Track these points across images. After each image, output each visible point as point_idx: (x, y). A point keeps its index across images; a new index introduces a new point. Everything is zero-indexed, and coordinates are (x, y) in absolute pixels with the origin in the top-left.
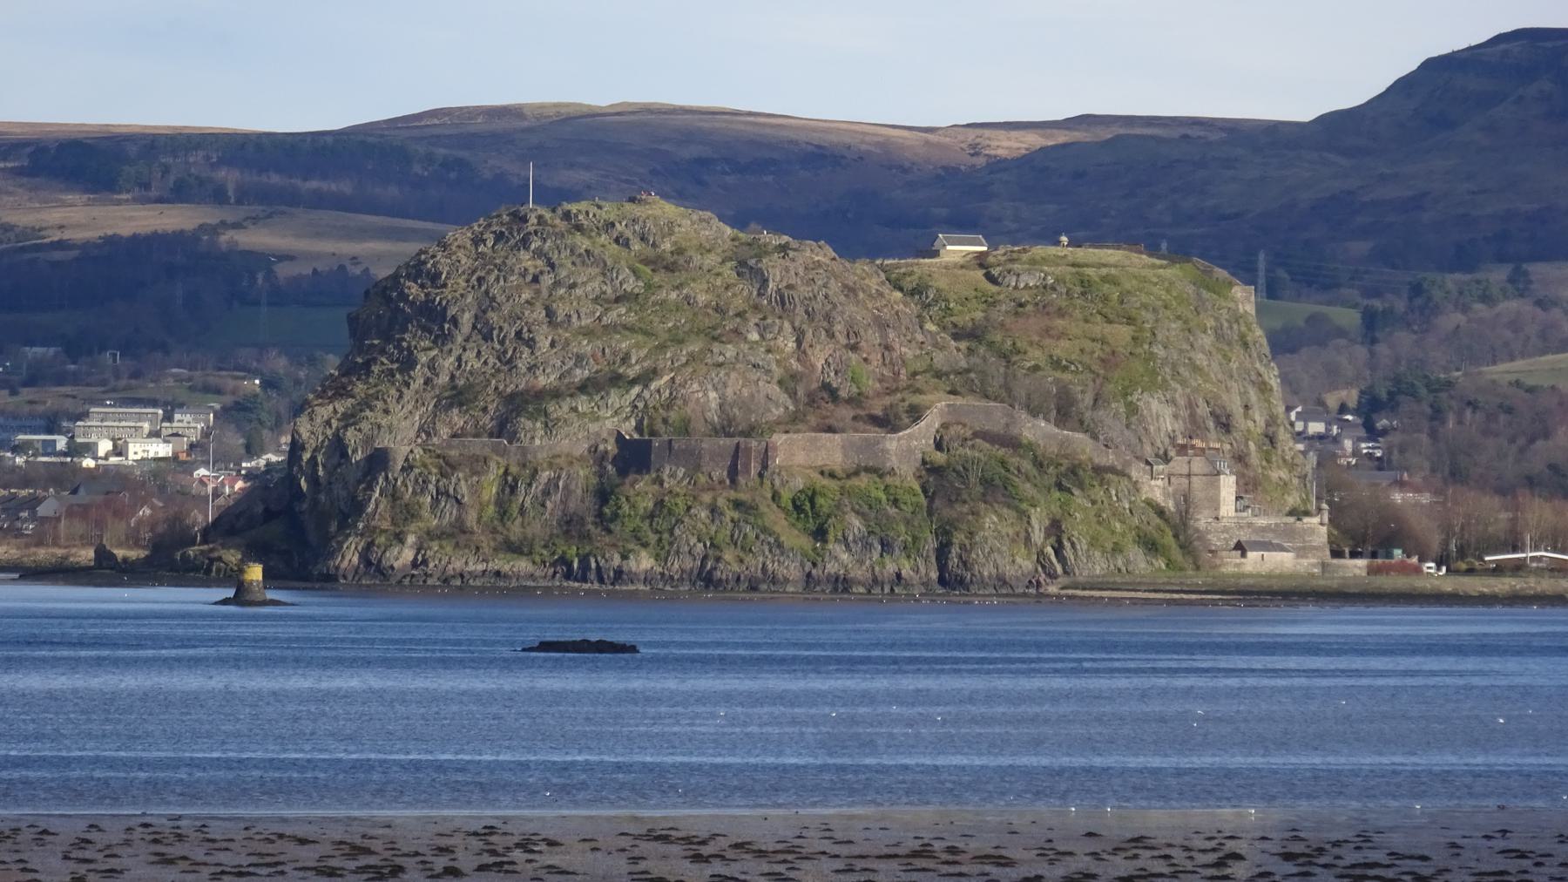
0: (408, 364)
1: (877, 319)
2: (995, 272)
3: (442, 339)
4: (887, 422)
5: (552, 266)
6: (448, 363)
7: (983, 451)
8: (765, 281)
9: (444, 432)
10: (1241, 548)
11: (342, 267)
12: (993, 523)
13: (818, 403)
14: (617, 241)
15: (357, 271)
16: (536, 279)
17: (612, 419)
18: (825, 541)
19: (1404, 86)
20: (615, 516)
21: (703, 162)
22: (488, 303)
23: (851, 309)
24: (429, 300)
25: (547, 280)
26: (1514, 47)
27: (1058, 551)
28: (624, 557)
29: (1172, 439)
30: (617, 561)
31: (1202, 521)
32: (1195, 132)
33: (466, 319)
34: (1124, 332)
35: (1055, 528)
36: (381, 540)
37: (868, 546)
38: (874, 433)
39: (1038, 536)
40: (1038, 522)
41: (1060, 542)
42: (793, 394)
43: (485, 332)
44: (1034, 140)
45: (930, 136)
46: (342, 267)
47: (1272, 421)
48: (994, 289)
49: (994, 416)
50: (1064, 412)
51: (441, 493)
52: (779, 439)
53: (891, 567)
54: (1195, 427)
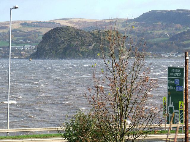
17: (65, 45)
33: (52, 37)
35: (104, 54)
43: (54, 38)
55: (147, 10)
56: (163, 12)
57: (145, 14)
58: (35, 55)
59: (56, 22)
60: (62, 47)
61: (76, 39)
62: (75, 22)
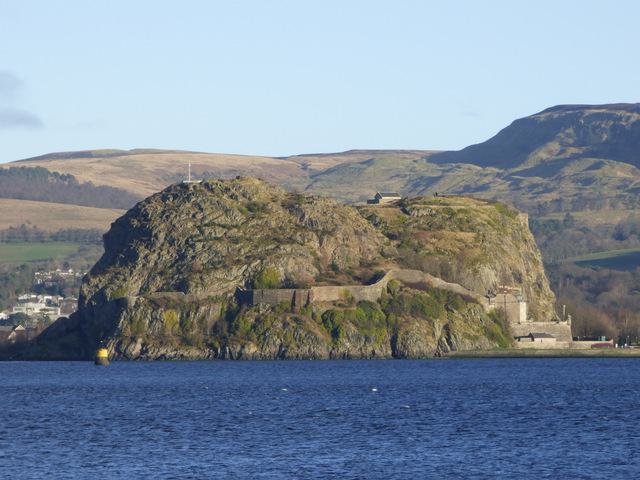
2: (408, 209)
3: (150, 245)
5: (202, 210)
6: (154, 257)
12: (418, 326)
13: (330, 274)
14: (231, 197)
17: (232, 280)
19: (505, 133)
25: (199, 216)
27: (448, 340)
29: (495, 286)
33: (162, 236)
34: (469, 236)
35: (446, 328)
39: (438, 333)
40: (439, 325)
45: (285, 162)
47: (539, 276)
49: (416, 276)
50: (445, 274)
51: (154, 319)
52: (315, 289)
54: (505, 281)
55: (532, 105)
56: (619, 113)
57: (517, 123)
58: (68, 331)
59: (52, 166)
60: (215, 290)
61: (288, 248)
62: (150, 167)
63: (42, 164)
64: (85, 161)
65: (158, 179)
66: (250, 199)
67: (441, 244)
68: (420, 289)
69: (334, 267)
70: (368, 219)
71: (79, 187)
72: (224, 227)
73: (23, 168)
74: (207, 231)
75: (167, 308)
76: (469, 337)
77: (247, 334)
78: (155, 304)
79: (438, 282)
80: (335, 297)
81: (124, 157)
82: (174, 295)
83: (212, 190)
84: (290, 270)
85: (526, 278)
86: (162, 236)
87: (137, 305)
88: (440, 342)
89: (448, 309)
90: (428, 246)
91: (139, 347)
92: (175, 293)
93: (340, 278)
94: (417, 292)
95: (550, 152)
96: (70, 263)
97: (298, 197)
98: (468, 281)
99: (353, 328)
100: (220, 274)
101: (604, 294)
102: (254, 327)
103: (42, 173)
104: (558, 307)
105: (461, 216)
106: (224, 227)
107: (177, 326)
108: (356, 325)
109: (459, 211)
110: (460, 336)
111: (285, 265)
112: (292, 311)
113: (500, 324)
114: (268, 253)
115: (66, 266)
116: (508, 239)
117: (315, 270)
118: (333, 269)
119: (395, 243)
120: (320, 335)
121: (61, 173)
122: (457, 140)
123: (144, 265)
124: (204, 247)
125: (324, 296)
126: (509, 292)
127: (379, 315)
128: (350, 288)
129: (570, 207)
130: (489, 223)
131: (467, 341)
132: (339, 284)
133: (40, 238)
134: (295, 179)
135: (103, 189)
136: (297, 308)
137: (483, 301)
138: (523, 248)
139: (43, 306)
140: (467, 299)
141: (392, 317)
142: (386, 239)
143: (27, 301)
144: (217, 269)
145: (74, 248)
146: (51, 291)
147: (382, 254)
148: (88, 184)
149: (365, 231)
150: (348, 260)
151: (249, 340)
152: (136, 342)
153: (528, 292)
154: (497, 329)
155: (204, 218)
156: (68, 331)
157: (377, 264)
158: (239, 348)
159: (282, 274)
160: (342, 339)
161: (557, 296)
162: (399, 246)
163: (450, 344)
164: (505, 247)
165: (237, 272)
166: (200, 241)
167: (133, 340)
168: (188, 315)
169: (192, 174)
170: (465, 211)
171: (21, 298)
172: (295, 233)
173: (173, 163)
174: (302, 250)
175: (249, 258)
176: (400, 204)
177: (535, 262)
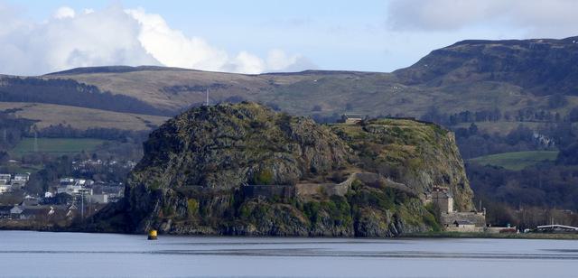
0: (166, 159)
1: (329, 144)
2: (367, 127)
3: (177, 151)
4: (337, 180)
5: (217, 126)
6: (180, 160)
7: (369, 190)
8: (291, 131)
9: (180, 183)
10: (457, 224)
11: (61, 125)
13: (310, 173)
14: (238, 117)
15: (66, 125)
16: (211, 130)
17: (237, 179)
18: (315, 222)
19: (425, 60)
20: (241, 213)
21: (177, 87)
22: (194, 139)
23: (321, 140)
24: (173, 137)
25: (215, 130)
26: (463, 46)
28: (245, 226)
29: (430, 185)
30: (242, 229)
31: (443, 214)
32: (174, 74)
33: (187, 144)
34: (411, 148)
35: (395, 216)
36: (160, 221)
37: (330, 223)
38: (329, 184)
39: (389, 220)
40: (389, 213)
41: (396, 221)
42: (302, 171)
43: (193, 148)
44: (292, 80)
46: (61, 125)
47: (462, 179)
48: (366, 133)
49: (373, 177)
50: (394, 175)
52: (299, 186)
53: (338, 230)
54: (438, 182)
59: (79, 78)
61: (280, 155)
63: (73, 77)
64: (104, 75)
65: (160, 90)
66: (251, 118)
67: (391, 154)
68: (376, 187)
69: (313, 170)
70: (338, 134)
71: (101, 95)
72: (233, 138)
73: (59, 80)
74: (220, 141)
75: (190, 198)
76: (411, 223)
77: (249, 218)
78: (181, 195)
79: (389, 182)
80: (314, 192)
81: (133, 73)
82: (194, 188)
83: (224, 112)
84: (281, 172)
85: (452, 180)
86: (187, 144)
87: (168, 196)
88: (390, 225)
89: (396, 203)
90: (381, 155)
91: (168, 226)
92: (195, 186)
93: (318, 178)
94: (374, 189)
95: (459, 76)
96: (98, 154)
97: (288, 118)
98: (411, 182)
99: (326, 214)
100: (229, 173)
101: (502, 187)
102: (254, 213)
103: (74, 83)
104: (475, 201)
105: (406, 133)
106: (233, 138)
107: (197, 210)
108: (329, 213)
109: (405, 130)
110: (405, 222)
111: (277, 169)
112: (282, 202)
113: (434, 214)
114: (264, 158)
115: (95, 157)
116: (440, 151)
117: (299, 171)
118: (313, 172)
119: (356, 153)
120: (302, 220)
121: (86, 84)
122: (388, 67)
123: (174, 166)
124: (218, 153)
125: (306, 191)
126: (441, 190)
127: (346, 205)
128: (325, 185)
129: (474, 118)
130: (426, 138)
131: (410, 226)
132: (317, 183)
133: (73, 134)
134: (265, 92)
135: (120, 97)
136: (285, 200)
137: (422, 196)
138: (451, 158)
139: (80, 188)
140: (411, 196)
141: (355, 207)
142: (351, 150)
143: (69, 183)
144: (227, 170)
145: (100, 142)
146: (87, 176)
147: (349, 161)
148: (108, 93)
149: (336, 144)
150: (323, 165)
151: (250, 221)
152: (167, 222)
153: (454, 191)
154: (432, 218)
155: (218, 131)
156: (117, 213)
157: (344, 168)
158: (242, 229)
159: (275, 174)
160: (319, 223)
161: (475, 193)
162: (360, 155)
163: (397, 227)
164: (438, 157)
165: (243, 171)
166: (214, 149)
167: (165, 221)
168: (205, 203)
169: (209, 97)
170: (409, 130)
171: (62, 180)
172: (285, 143)
173: (171, 78)
174: (290, 156)
175: (251, 162)
176: (361, 123)
177: (460, 168)
